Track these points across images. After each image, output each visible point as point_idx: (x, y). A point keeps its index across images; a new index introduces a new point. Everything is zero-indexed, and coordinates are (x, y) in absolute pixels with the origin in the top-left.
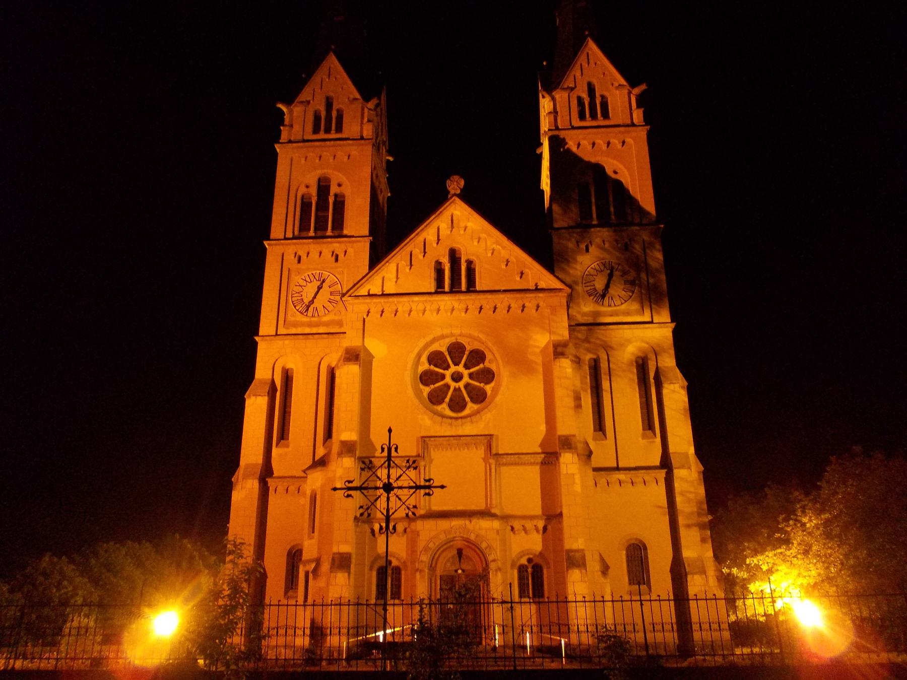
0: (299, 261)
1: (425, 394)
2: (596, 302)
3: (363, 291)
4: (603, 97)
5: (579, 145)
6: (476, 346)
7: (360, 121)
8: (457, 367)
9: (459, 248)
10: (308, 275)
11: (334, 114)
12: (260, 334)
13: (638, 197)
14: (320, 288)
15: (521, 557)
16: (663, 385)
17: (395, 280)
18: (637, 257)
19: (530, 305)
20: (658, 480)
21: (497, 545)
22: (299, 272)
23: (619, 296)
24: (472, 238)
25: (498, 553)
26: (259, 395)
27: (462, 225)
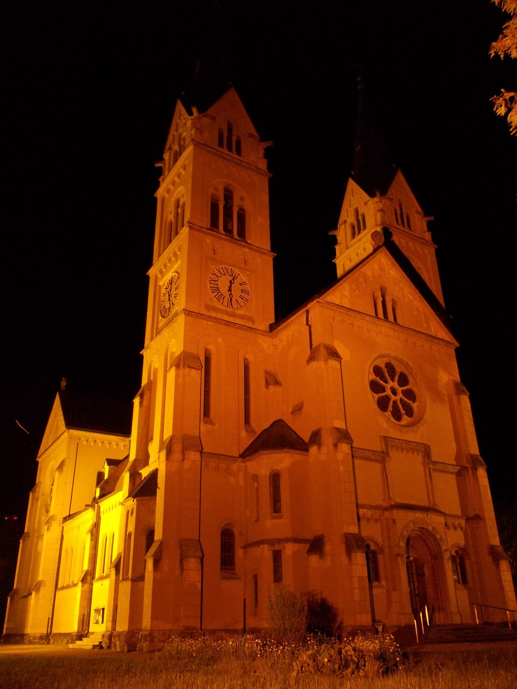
23: (237, 301)
26: (194, 368)
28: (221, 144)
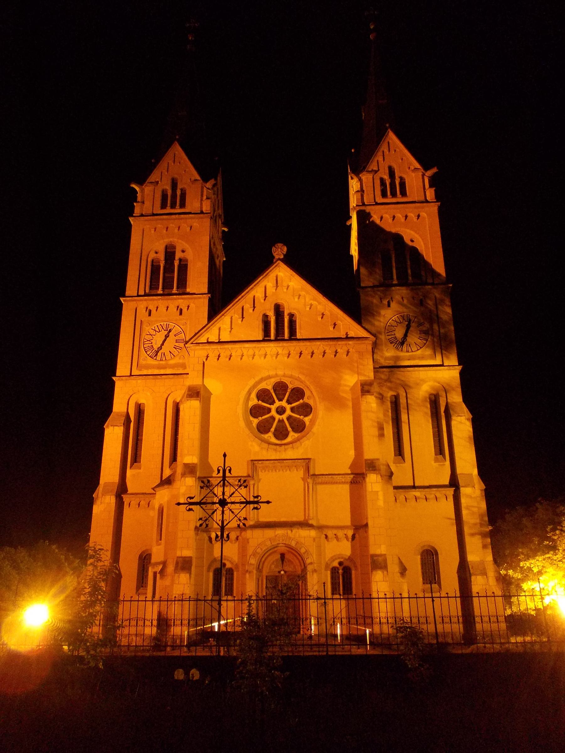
1: (255, 425)
4: (401, 178)
5: (382, 218)
6: (297, 384)
8: (281, 402)
10: (157, 326)
11: (179, 193)
12: (118, 374)
14: (167, 336)
15: (334, 561)
18: (430, 311)
21: (313, 550)
23: (416, 344)
27: (285, 284)
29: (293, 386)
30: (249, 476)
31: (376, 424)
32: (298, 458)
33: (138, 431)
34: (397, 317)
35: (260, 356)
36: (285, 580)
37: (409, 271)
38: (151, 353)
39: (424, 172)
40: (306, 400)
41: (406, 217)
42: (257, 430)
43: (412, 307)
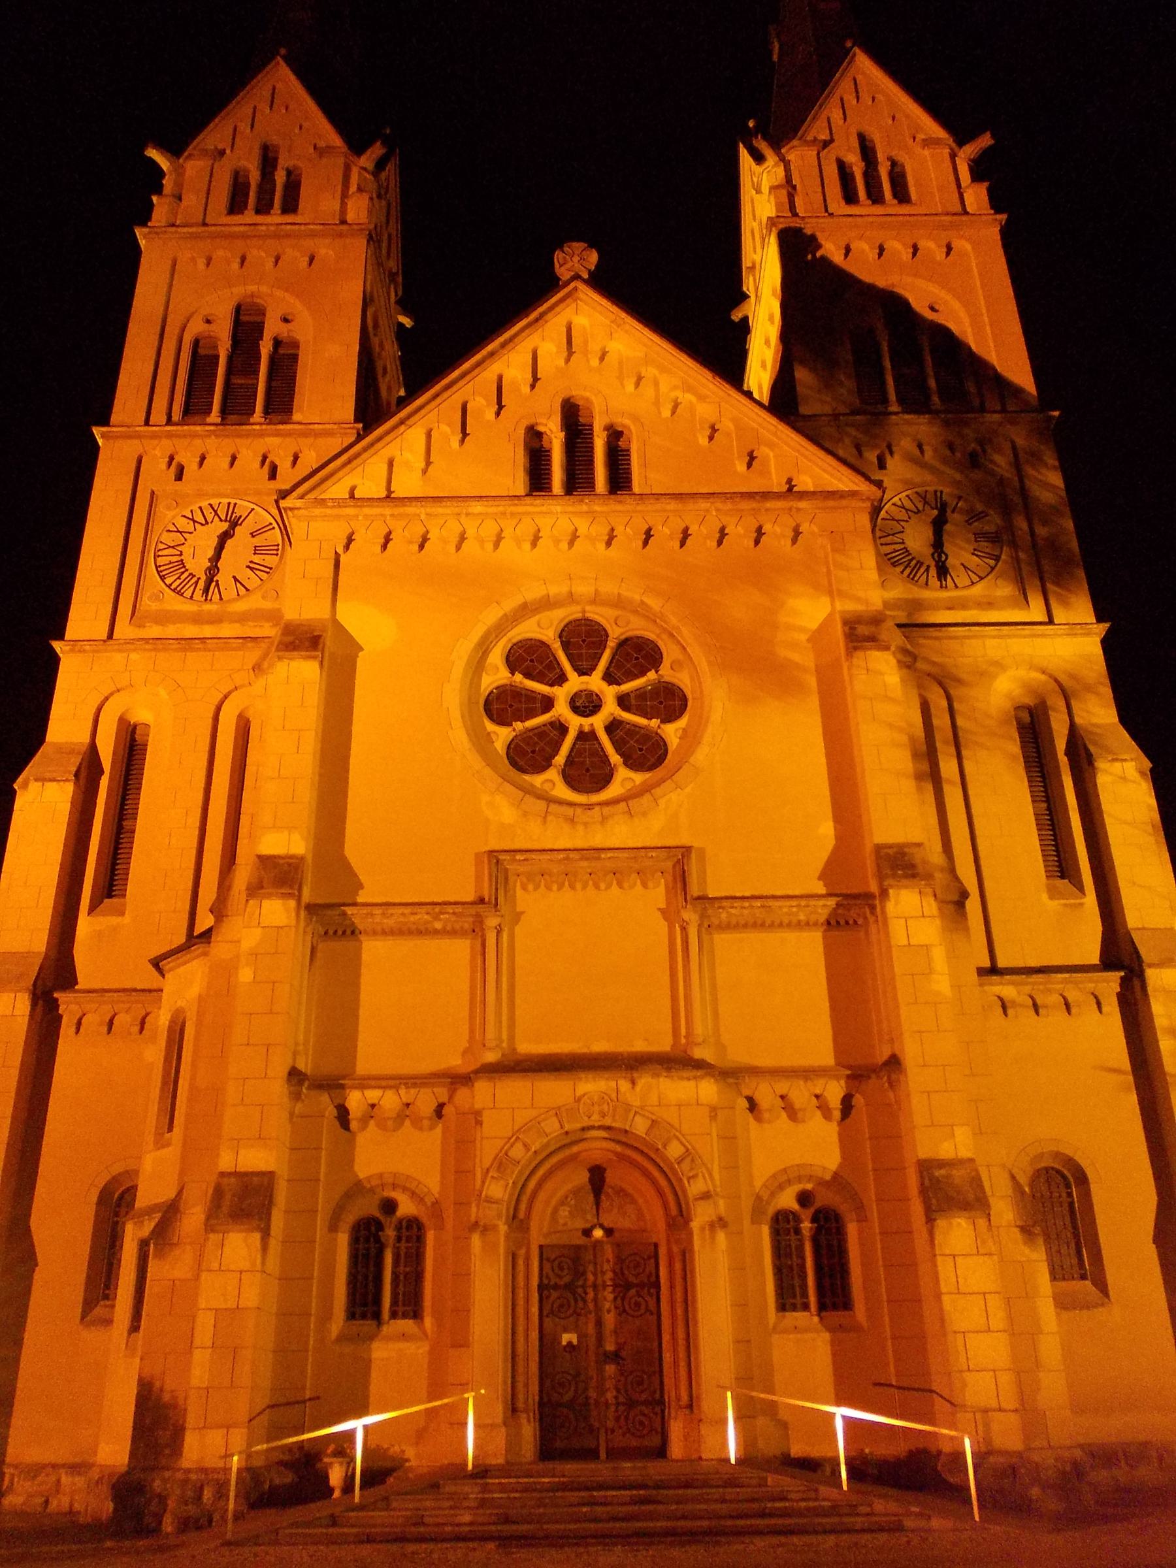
0: (179, 477)
1: (500, 745)
2: (912, 578)
3: (337, 489)
4: (894, 163)
5: (848, 250)
6: (638, 627)
7: (339, 188)
8: (585, 678)
9: (587, 400)
10: (200, 508)
11: (280, 178)
12: (69, 635)
13: (993, 358)
14: (224, 537)
15: (781, 1187)
16: (1096, 764)
17: (423, 465)
18: (1001, 481)
19: (777, 531)
20: (1100, 998)
21: (711, 1150)
22: (179, 501)
23: (964, 567)
24: (621, 378)
25: (717, 1176)
27: (595, 347)
28: (850, 197)
29: (622, 630)
30: (481, 901)
31: (904, 739)
32: (648, 844)
33: (123, 804)
34: (907, 496)
35: (518, 542)
36: (608, 1261)
37: (932, 383)
38: (178, 582)
39: (954, 145)
40: (666, 672)
41: (915, 249)
42: (506, 762)
43: (949, 471)
